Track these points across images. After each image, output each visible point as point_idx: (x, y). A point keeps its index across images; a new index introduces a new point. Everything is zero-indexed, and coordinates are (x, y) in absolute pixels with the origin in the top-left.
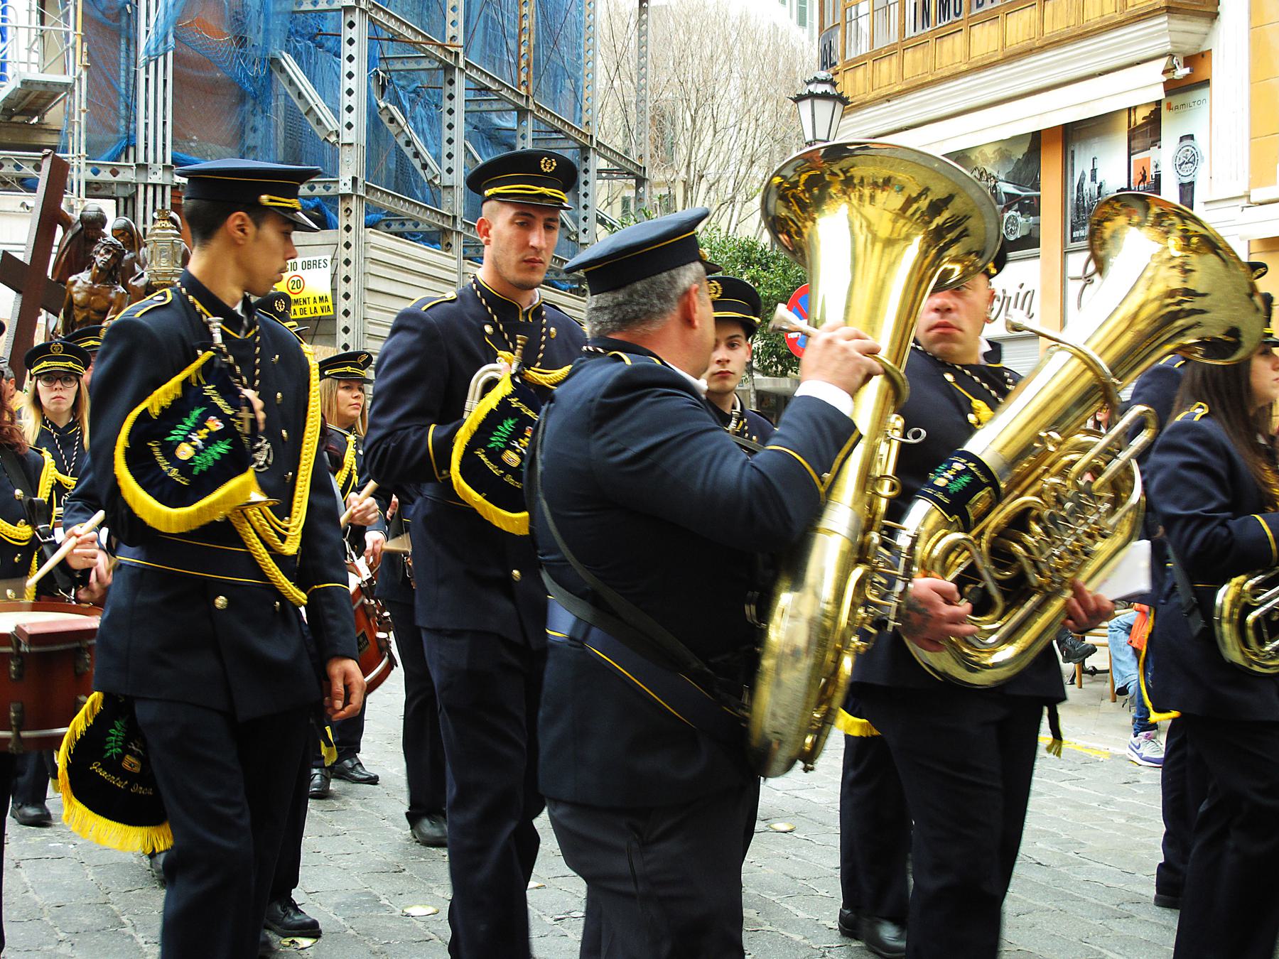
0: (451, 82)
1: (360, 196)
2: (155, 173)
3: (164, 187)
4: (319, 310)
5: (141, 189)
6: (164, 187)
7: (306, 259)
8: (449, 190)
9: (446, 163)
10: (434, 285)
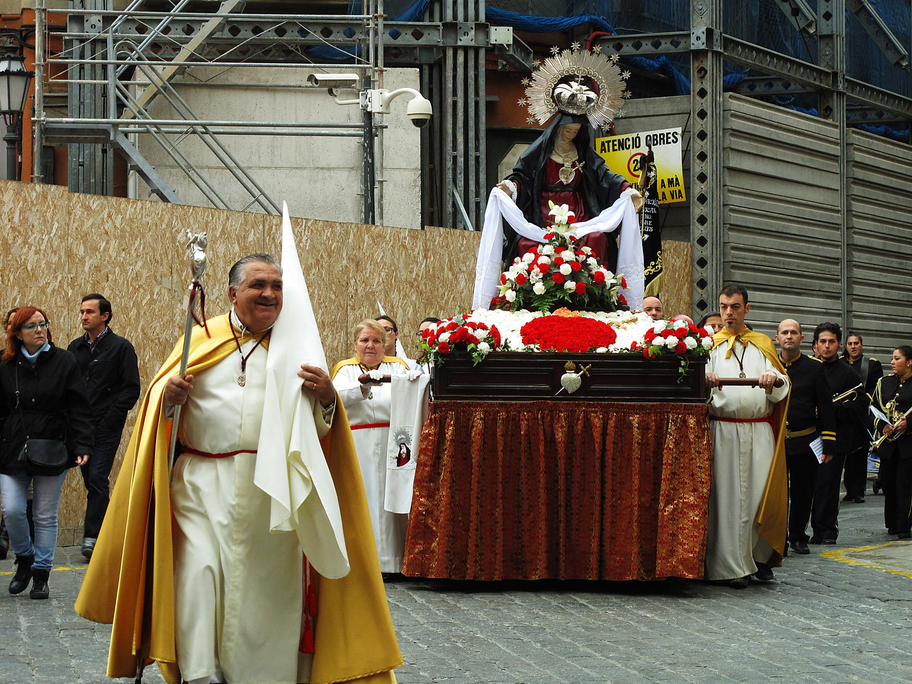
4: (668, 196)
5: (450, 53)
6: (476, 50)
7: (651, 133)
8: (827, 40)
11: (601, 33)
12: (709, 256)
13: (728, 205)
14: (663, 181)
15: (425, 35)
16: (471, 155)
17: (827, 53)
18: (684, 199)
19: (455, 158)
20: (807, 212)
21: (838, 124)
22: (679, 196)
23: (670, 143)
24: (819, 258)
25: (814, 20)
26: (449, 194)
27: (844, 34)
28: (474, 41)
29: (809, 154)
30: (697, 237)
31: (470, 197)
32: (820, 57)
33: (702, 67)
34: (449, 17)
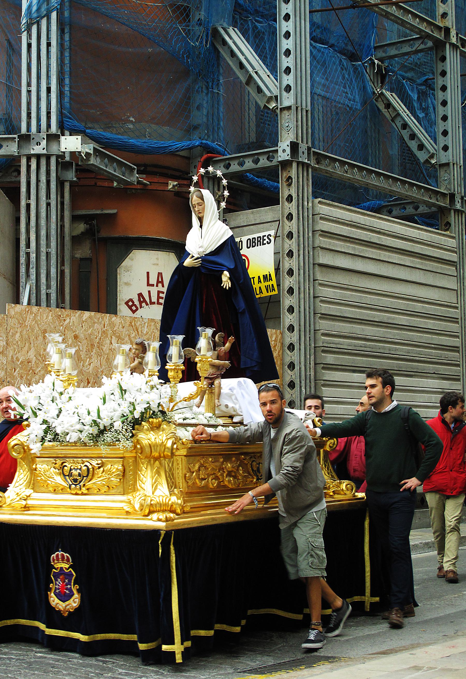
0: (443, 59)
1: (303, 164)
2: (38, 144)
3: (48, 157)
4: (264, 290)
5: (24, 161)
6: (48, 157)
7: (251, 237)
8: (445, 168)
9: (442, 141)
10: (422, 264)
11: (213, 155)
12: (296, 341)
13: (319, 297)
14: (259, 277)
15: (4, 147)
16: (42, 251)
17: (446, 178)
18: (276, 292)
19: (28, 254)
20: (418, 307)
21: (454, 235)
22: (272, 290)
23: (265, 244)
24: (433, 346)
25: (435, 152)
26: (22, 287)
27: (462, 162)
28: (45, 149)
29: (421, 258)
30: (287, 325)
31: (42, 289)
32: (441, 182)
33: (289, 176)
34: (24, 130)
